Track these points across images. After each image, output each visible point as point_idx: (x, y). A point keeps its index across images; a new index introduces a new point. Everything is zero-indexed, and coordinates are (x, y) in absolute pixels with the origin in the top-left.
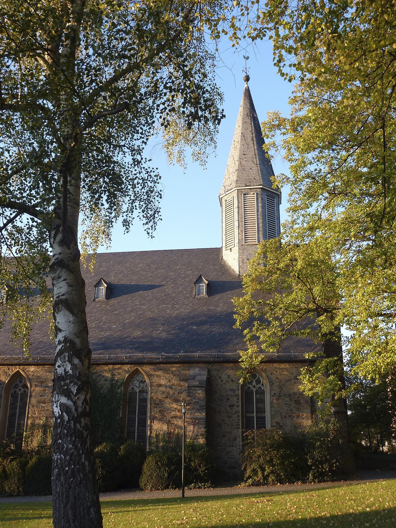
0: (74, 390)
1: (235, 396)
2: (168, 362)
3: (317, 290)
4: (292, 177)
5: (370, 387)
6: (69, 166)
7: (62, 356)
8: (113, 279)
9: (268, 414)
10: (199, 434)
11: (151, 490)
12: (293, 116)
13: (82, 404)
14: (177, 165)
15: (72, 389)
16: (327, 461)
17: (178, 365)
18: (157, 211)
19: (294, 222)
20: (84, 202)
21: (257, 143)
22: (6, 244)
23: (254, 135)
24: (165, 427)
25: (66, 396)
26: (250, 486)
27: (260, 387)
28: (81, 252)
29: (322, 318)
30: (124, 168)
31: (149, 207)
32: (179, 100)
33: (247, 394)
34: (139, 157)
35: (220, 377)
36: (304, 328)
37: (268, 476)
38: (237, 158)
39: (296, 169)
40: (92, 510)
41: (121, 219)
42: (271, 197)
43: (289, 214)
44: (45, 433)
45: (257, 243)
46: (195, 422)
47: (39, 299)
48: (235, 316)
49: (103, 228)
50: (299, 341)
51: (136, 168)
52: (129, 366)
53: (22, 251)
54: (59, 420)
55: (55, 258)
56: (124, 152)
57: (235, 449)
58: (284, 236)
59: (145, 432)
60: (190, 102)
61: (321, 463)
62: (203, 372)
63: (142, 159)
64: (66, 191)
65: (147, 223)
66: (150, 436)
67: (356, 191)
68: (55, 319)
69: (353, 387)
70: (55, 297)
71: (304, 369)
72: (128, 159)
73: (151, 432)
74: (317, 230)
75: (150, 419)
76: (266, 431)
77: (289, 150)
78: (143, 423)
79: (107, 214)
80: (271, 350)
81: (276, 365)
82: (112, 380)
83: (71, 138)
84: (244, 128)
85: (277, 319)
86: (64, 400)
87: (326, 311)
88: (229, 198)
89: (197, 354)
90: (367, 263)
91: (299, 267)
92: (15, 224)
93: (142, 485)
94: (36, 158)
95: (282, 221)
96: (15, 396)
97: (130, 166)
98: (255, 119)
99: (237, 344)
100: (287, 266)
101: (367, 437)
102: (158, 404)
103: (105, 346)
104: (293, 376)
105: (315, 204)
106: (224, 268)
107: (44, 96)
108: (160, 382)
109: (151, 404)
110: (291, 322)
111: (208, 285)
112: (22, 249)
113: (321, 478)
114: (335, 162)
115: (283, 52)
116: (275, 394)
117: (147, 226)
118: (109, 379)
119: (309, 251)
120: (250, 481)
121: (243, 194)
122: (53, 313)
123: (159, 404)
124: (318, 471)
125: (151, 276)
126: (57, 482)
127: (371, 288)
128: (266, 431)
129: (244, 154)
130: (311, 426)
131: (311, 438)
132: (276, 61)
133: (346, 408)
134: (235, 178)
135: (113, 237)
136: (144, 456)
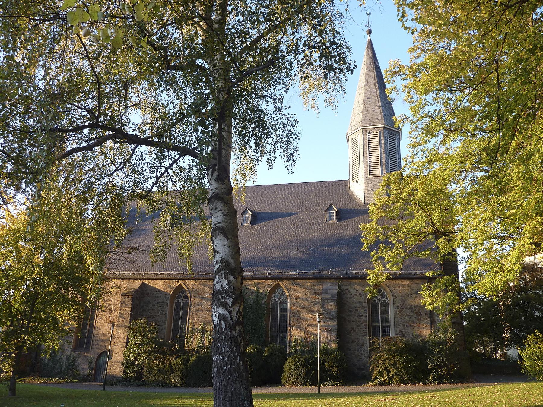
0: (230, 302)
1: (363, 308)
2: (303, 278)
3: (436, 216)
4: (412, 117)
5: (484, 301)
6: (223, 116)
7: (220, 274)
8: (256, 208)
9: (392, 324)
10: (332, 340)
11: (291, 386)
12: (412, 63)
13: (237, 314)
14: (312, 110)
15: (228, 302)
16: (445, 365)
17: (313, 281)
18: (296, 151)
19: (414, 156)
20: (234, 145)
21: (379, 88)
22: (172, 181)
23: (376, 81)
24: (302, 334)
25: (223, 307)
26: (376, 385)
27: (384, 300)
28: (233, 185)
29: (441, 240)
30: (268, 115)
31: (289, 147)
32: (316, 55)
33: (373, 306)
34: (280, 105)
35: (349, 292)
36: (424, 250)
37: (393, 377)
38: (361, 101)
39: (415, 110)
40: (246, 402)
41: (265, 158)
42: (392, 134)
43: (410, 149)
44: (203, 335)
45: (380, 175)
46: (328, 330)
47: (198, 224)
48: (363, 240)
49: (250, 166)
50: (419, 261)
51: (278, 114)
52: (271, 281)
53: (185, 187)
54: (218, 328)
55: (212, 192)
56: (267, 101)
57: (363, 353)
58: (406, 168)
59: (285, 337)
60: (325, 56)
61: (440, 367)
62: (334, 287)
63: (282, 106)
64: (220, 137)
65: (287, 161)
66: (290, 341)
67: (471, 128)
68: (213, 243)
69: (470, 301)
70: (213, 225)
71: (424, 286)
72: (271, 107)
73: (290, 337)
74: (435, 163)
75: (290, 326)
76: (390, 339)
77: (409, 93)
78: (283, 330)
79: (254, 154)
80: (395, 269)
81: (399, 282)
82: (258, 293)
83: (223, 91)
84: (368, 76)
85: (399, 242)
86: (221, 311)
87: (444, 234)
88: (355, 136)
89: (328, 272)
90: (482, 192)
91: (419, 196)
92: (179, 164)
93: (283, 381)
94: (195, 109)
95: (403, 155)
96: (178, 305)
97: (272, 113)
98: (377, 67)
99: (364, 263)
100: (409, 195)
101: (481, 345)
102: (296, 314)
103: (252, 264)
104: (414, 291)
105: (433, 140)
106: (351, 198)
107: (200, 56)
108: (296, 295)
109: (290, 314)
110: (412, 245)
111: (338, 213)
112: (185, 185)
113: (440, 380)
114: (451, 102)
115: (406, 9)
116: (398, 306)
117: (287, 164)
118: (254, 292)
119: (429, 182)
120: (377, 381)
121: (367, 133)
122: (212, 238)
123: (296, 314)
124: (437, 374)
125: (288, 205)
126: (217, 379)
127: (488, 215)
128: (390, 339)
129: (368, 98)
130: (430, 336)
131: (431, 346)
132: (399, 17)
133: (462, 319)
134: (360, 119)
135: (259, 172)
136: (284, 358)
